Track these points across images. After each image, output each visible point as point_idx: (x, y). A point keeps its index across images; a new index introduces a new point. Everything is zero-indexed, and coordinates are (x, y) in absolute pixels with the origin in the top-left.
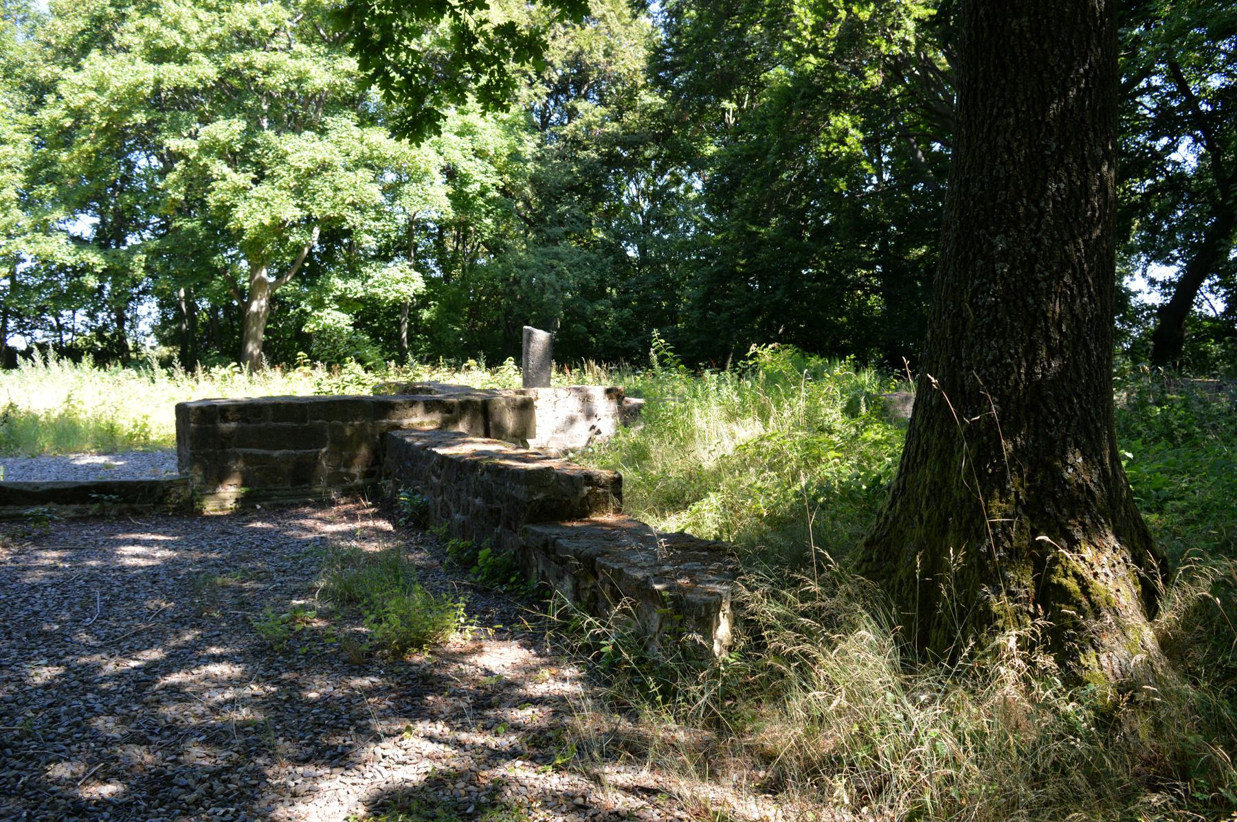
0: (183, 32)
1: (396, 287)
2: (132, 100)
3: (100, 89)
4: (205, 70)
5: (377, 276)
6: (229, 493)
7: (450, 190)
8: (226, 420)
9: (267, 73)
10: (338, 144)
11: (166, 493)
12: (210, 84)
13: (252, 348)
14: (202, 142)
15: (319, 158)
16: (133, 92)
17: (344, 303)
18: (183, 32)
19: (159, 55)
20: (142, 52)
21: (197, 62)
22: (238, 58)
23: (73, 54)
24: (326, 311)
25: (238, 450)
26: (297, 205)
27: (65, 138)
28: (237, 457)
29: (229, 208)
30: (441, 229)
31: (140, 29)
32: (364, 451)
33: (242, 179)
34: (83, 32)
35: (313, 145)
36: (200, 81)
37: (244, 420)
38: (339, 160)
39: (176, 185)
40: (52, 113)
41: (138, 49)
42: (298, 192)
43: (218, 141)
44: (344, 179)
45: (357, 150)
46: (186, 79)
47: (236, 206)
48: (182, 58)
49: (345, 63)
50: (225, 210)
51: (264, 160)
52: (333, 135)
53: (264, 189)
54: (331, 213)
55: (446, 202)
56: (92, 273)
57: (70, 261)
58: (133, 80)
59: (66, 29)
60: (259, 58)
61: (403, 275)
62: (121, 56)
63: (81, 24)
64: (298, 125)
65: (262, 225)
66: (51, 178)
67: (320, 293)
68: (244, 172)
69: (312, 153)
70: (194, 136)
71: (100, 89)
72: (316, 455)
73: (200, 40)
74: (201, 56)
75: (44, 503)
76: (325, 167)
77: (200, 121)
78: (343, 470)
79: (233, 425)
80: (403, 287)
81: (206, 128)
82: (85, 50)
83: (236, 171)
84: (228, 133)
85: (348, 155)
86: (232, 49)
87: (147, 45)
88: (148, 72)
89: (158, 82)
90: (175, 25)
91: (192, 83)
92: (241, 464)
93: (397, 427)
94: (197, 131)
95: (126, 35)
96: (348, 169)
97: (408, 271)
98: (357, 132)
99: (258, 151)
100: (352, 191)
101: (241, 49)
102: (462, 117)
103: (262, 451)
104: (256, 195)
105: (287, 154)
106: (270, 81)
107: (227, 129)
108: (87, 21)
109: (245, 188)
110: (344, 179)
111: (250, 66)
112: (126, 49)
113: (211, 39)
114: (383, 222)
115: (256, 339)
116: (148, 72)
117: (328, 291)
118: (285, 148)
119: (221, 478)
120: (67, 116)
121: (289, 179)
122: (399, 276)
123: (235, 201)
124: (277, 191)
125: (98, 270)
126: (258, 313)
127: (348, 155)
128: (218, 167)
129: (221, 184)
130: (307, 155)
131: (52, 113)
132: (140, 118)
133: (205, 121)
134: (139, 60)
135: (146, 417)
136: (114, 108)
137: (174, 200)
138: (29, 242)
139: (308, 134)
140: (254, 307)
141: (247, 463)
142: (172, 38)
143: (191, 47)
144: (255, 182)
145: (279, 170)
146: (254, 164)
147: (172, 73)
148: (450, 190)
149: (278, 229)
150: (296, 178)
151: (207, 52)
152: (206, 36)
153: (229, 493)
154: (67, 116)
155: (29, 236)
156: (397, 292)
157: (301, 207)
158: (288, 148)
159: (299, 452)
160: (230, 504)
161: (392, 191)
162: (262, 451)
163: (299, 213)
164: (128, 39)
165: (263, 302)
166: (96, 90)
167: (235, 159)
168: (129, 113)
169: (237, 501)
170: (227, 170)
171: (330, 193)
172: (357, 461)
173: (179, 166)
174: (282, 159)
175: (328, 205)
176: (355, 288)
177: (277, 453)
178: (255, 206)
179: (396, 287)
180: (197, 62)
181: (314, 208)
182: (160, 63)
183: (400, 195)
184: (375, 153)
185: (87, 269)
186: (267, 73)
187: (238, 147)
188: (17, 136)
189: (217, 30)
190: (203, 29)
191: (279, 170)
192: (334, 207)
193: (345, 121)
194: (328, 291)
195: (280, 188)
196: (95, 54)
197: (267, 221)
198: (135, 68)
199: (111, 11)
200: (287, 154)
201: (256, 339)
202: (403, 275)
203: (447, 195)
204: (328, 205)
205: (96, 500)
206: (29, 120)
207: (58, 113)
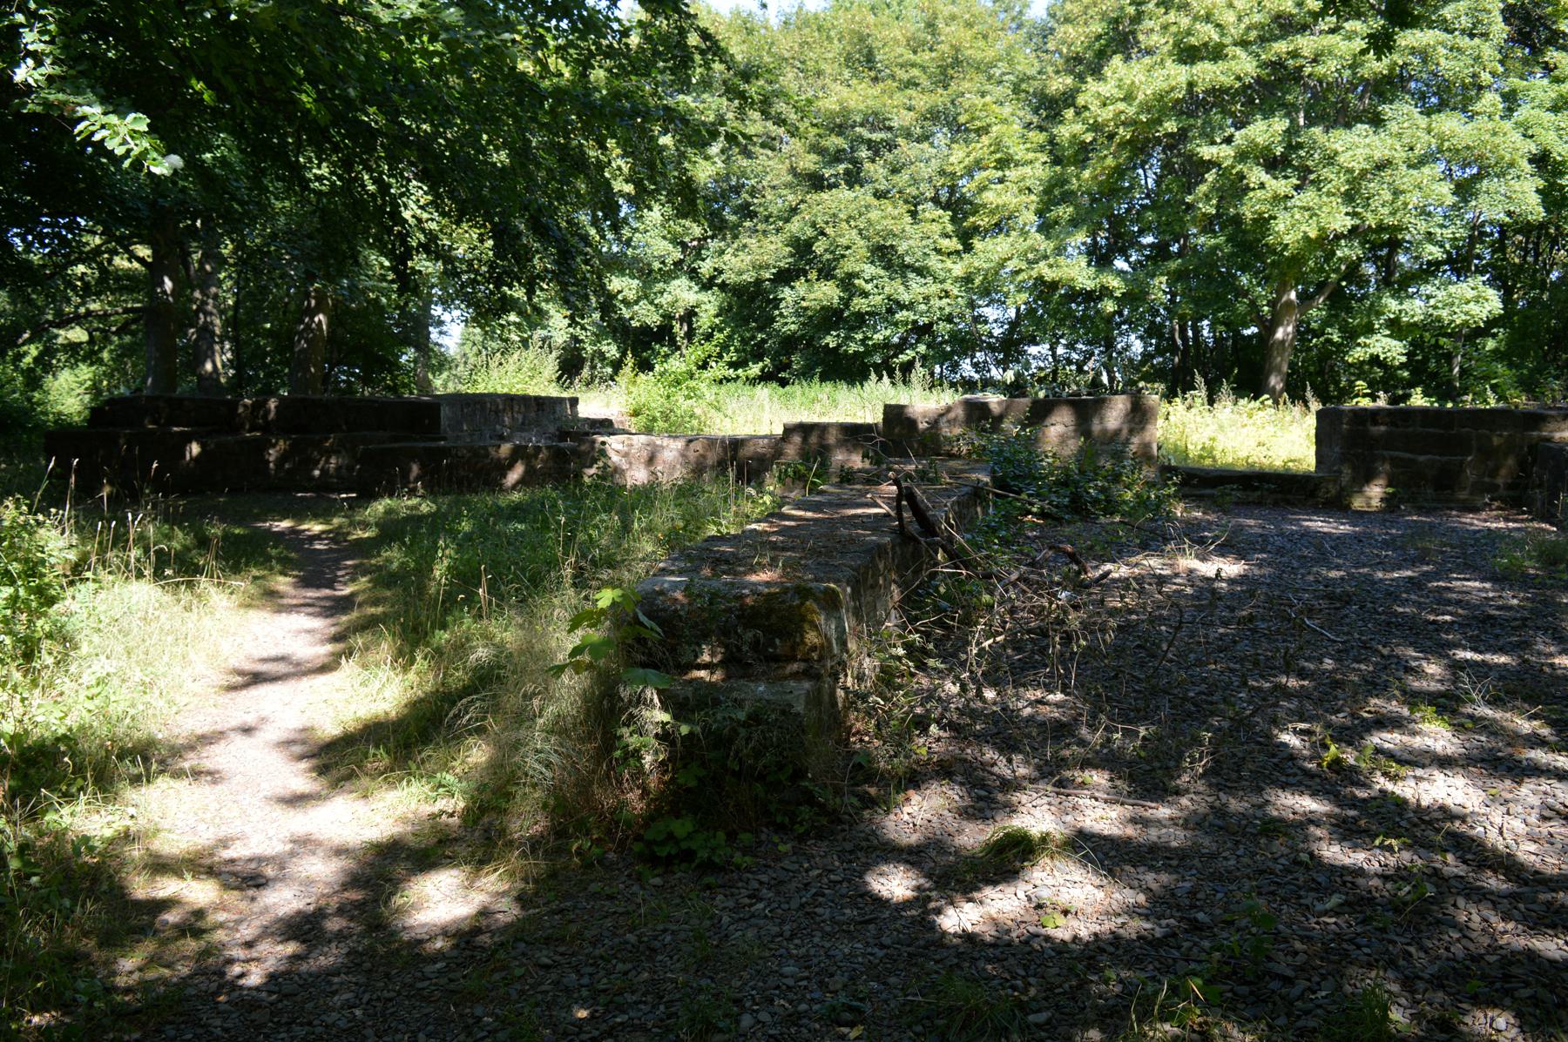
0: (1218, 25)
1: (1466, 308)
2: (1162, 106)
3: (1128, 98)
4: (1245, 65)
5: (1441, 295)
6: (1375, 492)
7: (1541, 183)
8: (1375, 423)
9: (1315, 60)
10: (1399, 135)
11: (1317, 487)
12: (1248, 80)
13: (1275, 381)
14: (1238, 146)
15: (1377, 155)
16: (1160, 97)
17: (1396, 328)
18: (1218, 25)
19: (1188, 54)
20: (1170, 54)
21: (1234, 57)
22: (1281, 47)
23: (1089, 65)
24: (1375, 337)
25: (1385, 453)
26: (1347, 214)
27: (1083, 153)
28: (1384, 460)
29: (1267, 221)
30: (1502, 233)
31: (1165, 27)
32: (1511, 461)
33: (1282, 186)
34: (1099, 37)
35: (1367, 141)
36: (1239, 78)
37: (1393, 424)
38: (1400, 155)
39: (1207, 197)
40: (1069, 129)
41: (1166, 49)
42: (1349, 197)
43: (1257, 145)
44: (1405, 177)
45: (1424, 142)
46: (1222, 78)
47: (1275, 218)
48: (1216, 53)
49: (1410, 37)
50: (1263, 223)
51: (1309, 163)
52: (1393, 127)
53: (1309, 197)
54: (1390, 221)
55: (1534, 199)
56: (1111, 296)
57: (1090, 285)
58: (1165, 86)
59: (1077, 36)
60: (1305, 44)
61: (1475, 293)
62: (1147, 60)
63: (1097, 28)
64: (1344, 118)
65: (1306, 238)
66: (1067, 197)
67: (1369, 316)
68: (1286, 177)
69: (1367, 151)
70: (1228, 140)
71: (1128, 98)
72: (1462, 463)
73: (1235, 32)
74: (1238, 51)
75: (1214, 487)
76: (1382, 166)
77: (1234, 125)
78: (1487, 479)
79: (1383, 428)
80: (1474, 308)
81: (1243, 131)
82: (1102, 56)
83: (1276, 178)
84: (1266, 136)
85: (1411, 149)
86: (1276, 39)
87: (1176, 45)
88: (1179, 75)
89: (1191, 85)
90: (1208, 18)
91: (1228, 81)
92: (1387, 467)
93: (1549, 440)
94: (1232, 136)
95: (1153, 33)
96: (1409, 167)
97: (1481, 288)
98: (1423, 121)
99: (1302, 153)
100: (1417, 193)
101: (1283, 37)
102: (1555, 87)
103: (1408, 455)
104: (1299, 203)
105: (1336, 153)
106: (1320, 70)
107: (1266, 131)
108: (1104, 24)
109: (1287, 197)
110: (1405, 177)
111: (1295, 54)
112: (1149, 52)
113: (1248, 28)
114: (1452, 229)
115: (1279, 371)
116: (1179, 75)
117: (1379, 314)
118: (1334, 147)
119: (1368, 478)
120: (1088, 130)
121: (1339, 183)
122: (1470, 294)
123: (1275, 212)
124: (1325, 199)
125: (1118, 294)
126: (1283, 342)
127: (1411, 149)
128: (1256, 175)
129: (1259, 193)
130: (1361, 152)
131: (1069, 129)
132: (1171, 126)
133: (1240, 125)
134: (1169, 63)
135: (1213, 439)
136: (1143, 118)
137: (1204, 214)
138: (1051, 266)
139: (1361, 128)
140: (1280, 334)
141: (1393, 466)
142: (1207, 33)
143: (1227, 41)
144: (1297, 188)
145: (1326, 173)
146: (1295, 169)
147: (1208, 73)
148: (1541, 183)
149: (1325, 243)
150: (1348, 181)
151: (1243, 43)
152: (1243, 26)
153: (1375, 492)
154: (1088, 130)
155: (1051, 260)
156: (1466, 314)
157: (1354, 215)
158: (1338, 147)
159: (1445, 458)
160: (1376, 503)
161: (1465, 190)
162: (1408, 455)
163: (1349, 222)
164: (1155, 39)
165: (1290, 329)
166: (1123, 100)
167: (1274, 164)
168: (1159, 122)
169: (1382, 500)
170: (1265, 177)
171: (1388, 196)
172: (1503, 472)
173: (1210, 177)
174: (1330, 159)
175: (1385, 211)
176: (1414, 309)
177: (1422, 458)
178: (1297, 216)
179: (1466, 308)
180: (1234, 57)
181: (1369, 215)
182: (1193, 63)
183: (1475, 195)
184: (1446, 144)
185: (1105, 292)
186: (1315, 60)
187: (1279, 151)
188: (1031, 156)
189: (1257, 18)
190: (1240, 19)
191: (1326, 173)
192: (1393, 214)
193: (1406, 108)
194: (1379, 314)
195: (1329, 194)
196: (1117, 60)
197: (1313, 234)
198: (1165, 72)
199: (1131, 10)
200: (1336, 153)
201: (1279, 371)
202: (1475, 293)
203: (1538, 191)
204: (1385, 211)
205: (1257, 488)
206: (1041, 138)
207: (1078, 128)
